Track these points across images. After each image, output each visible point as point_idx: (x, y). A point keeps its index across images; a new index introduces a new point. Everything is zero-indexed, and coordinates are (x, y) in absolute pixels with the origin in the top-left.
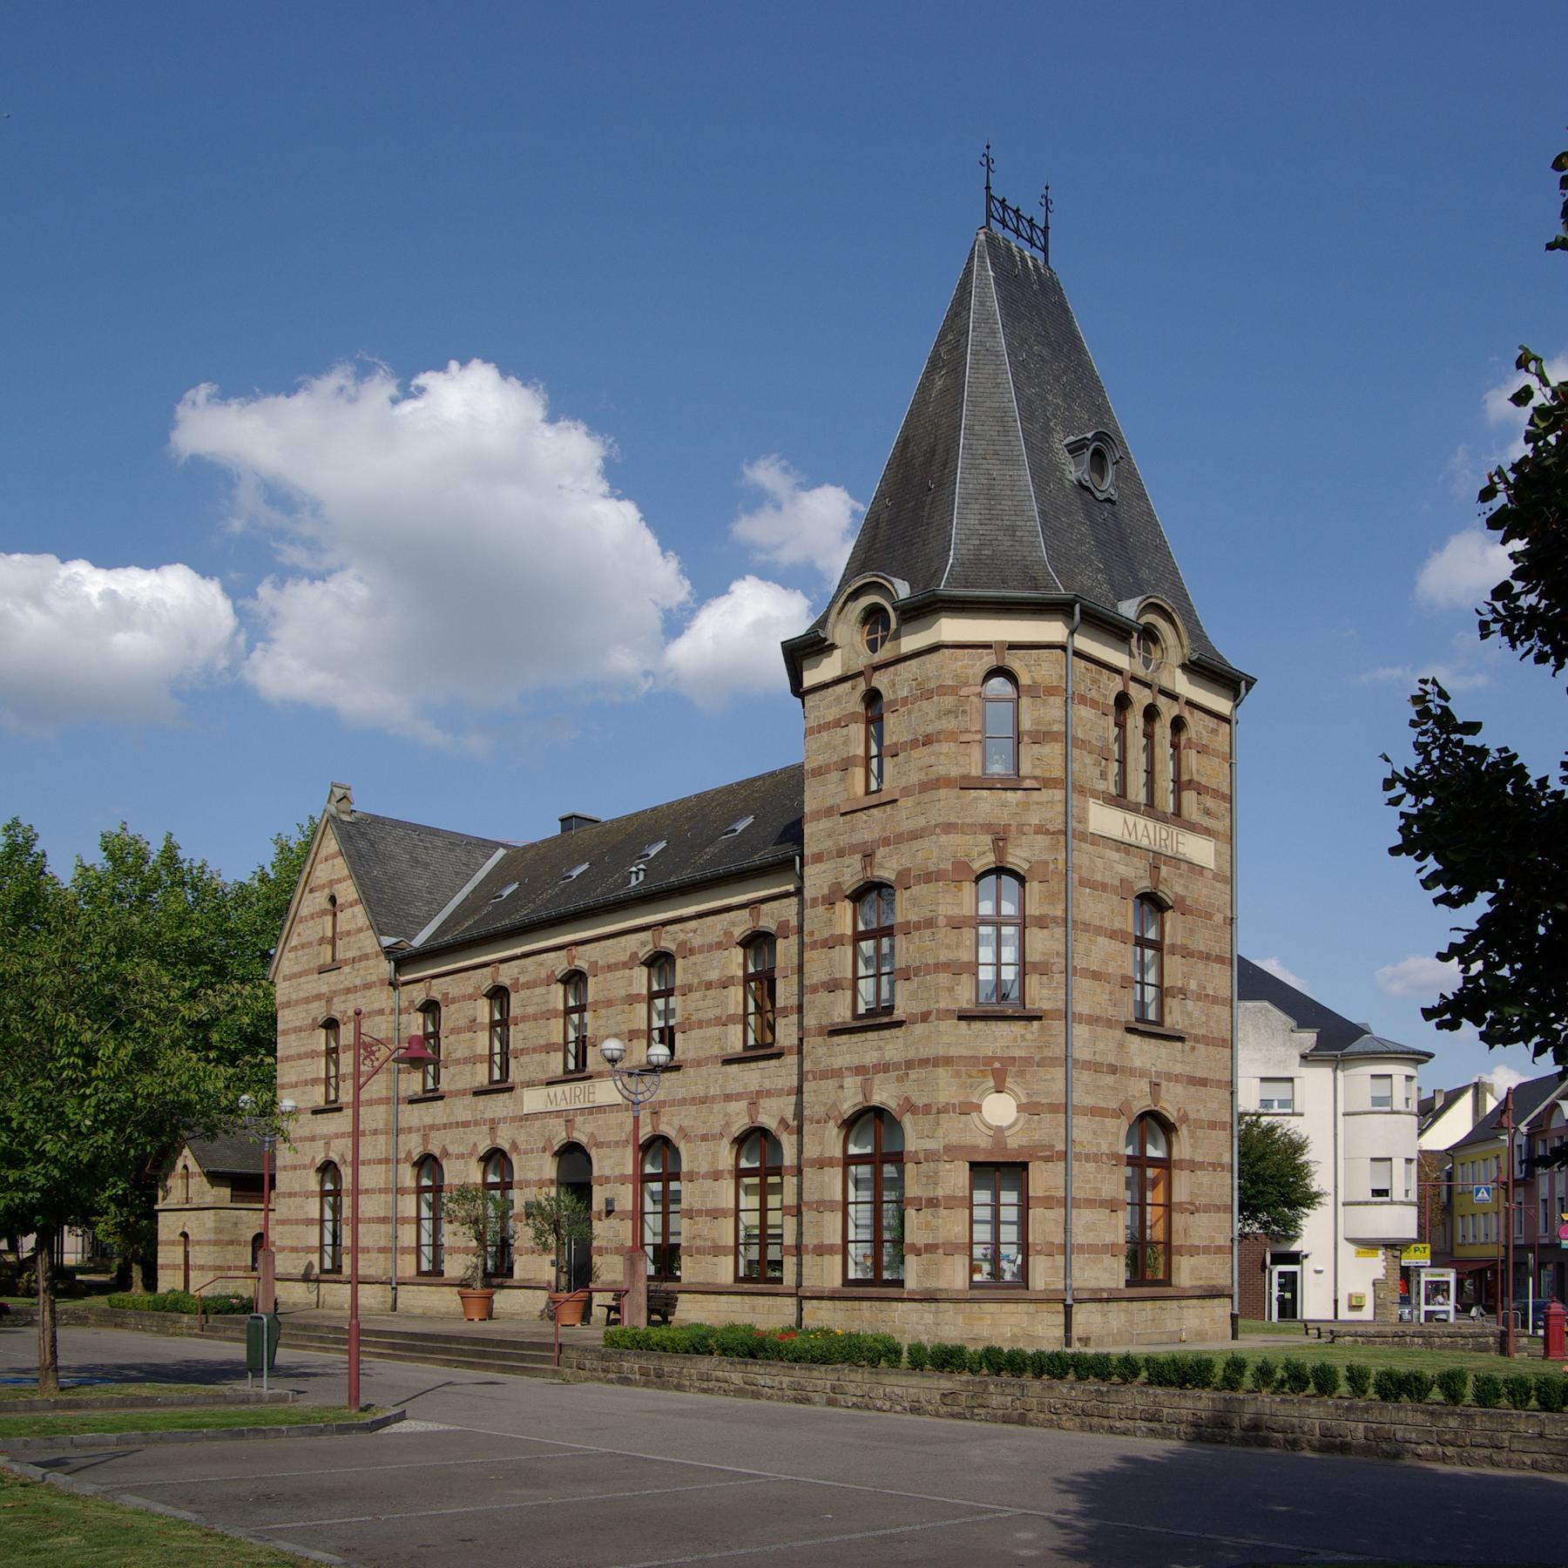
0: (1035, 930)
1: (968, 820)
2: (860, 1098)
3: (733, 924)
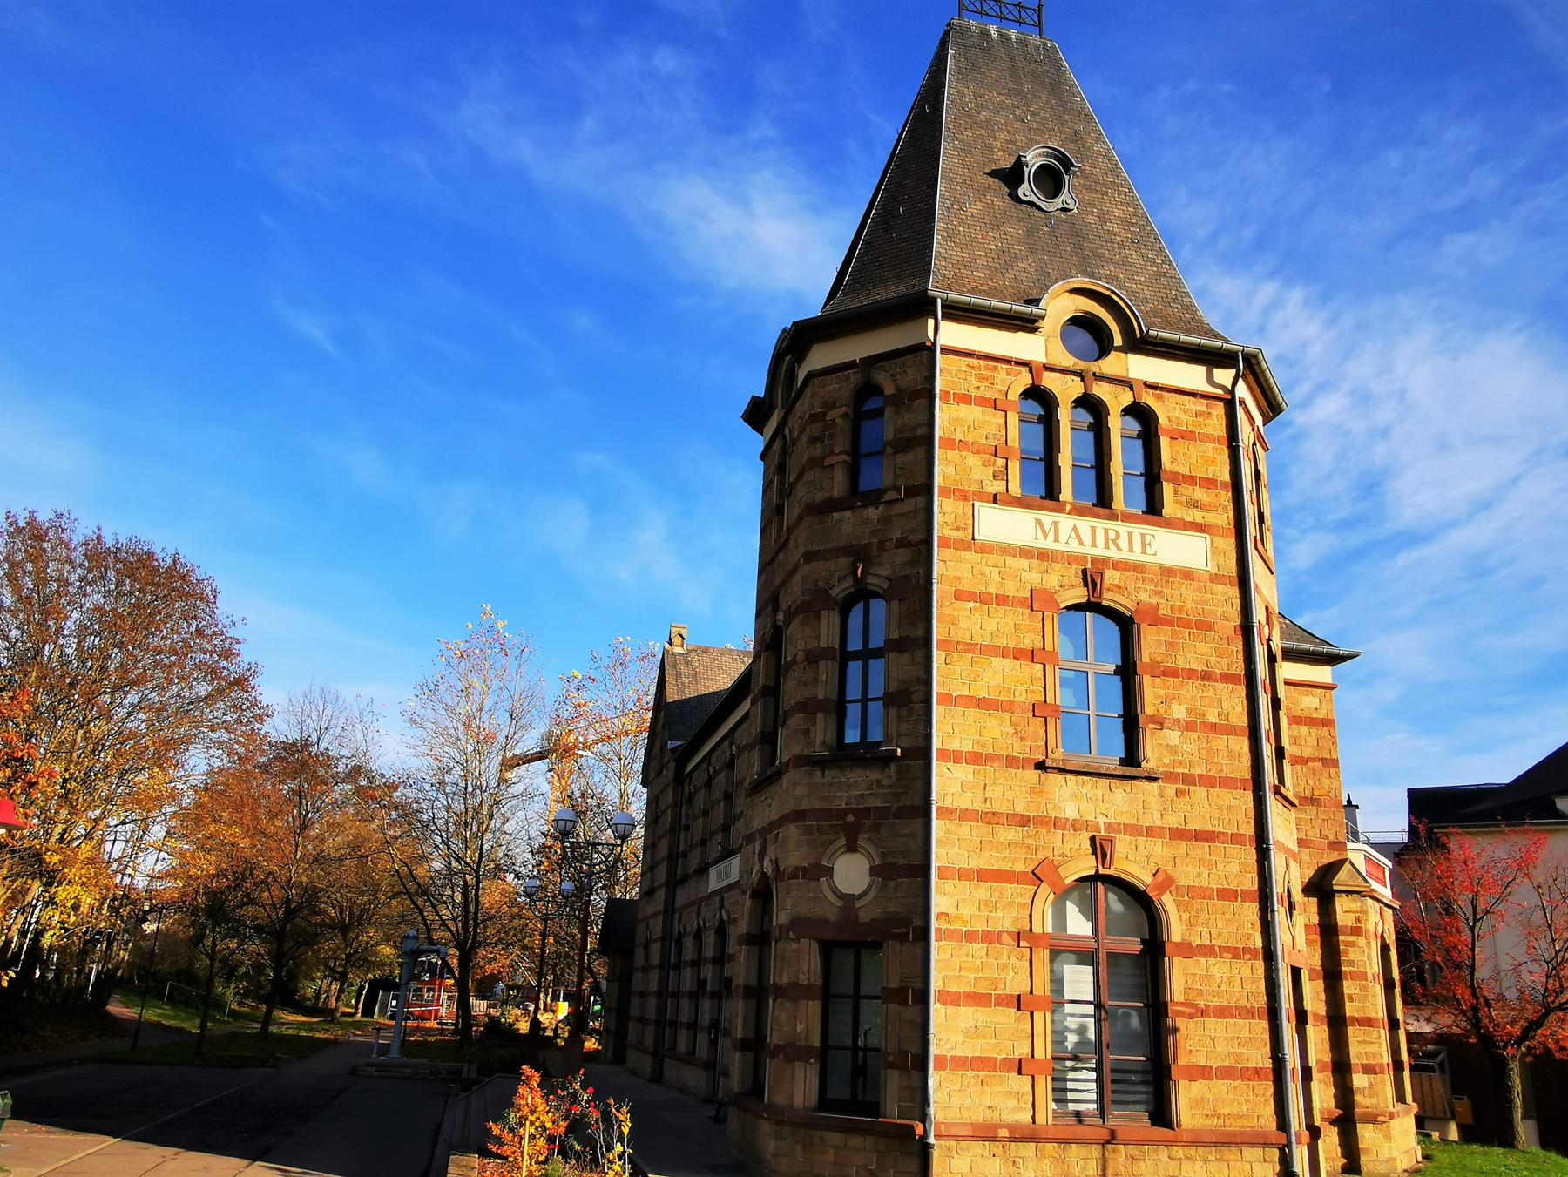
1: (829, 546)
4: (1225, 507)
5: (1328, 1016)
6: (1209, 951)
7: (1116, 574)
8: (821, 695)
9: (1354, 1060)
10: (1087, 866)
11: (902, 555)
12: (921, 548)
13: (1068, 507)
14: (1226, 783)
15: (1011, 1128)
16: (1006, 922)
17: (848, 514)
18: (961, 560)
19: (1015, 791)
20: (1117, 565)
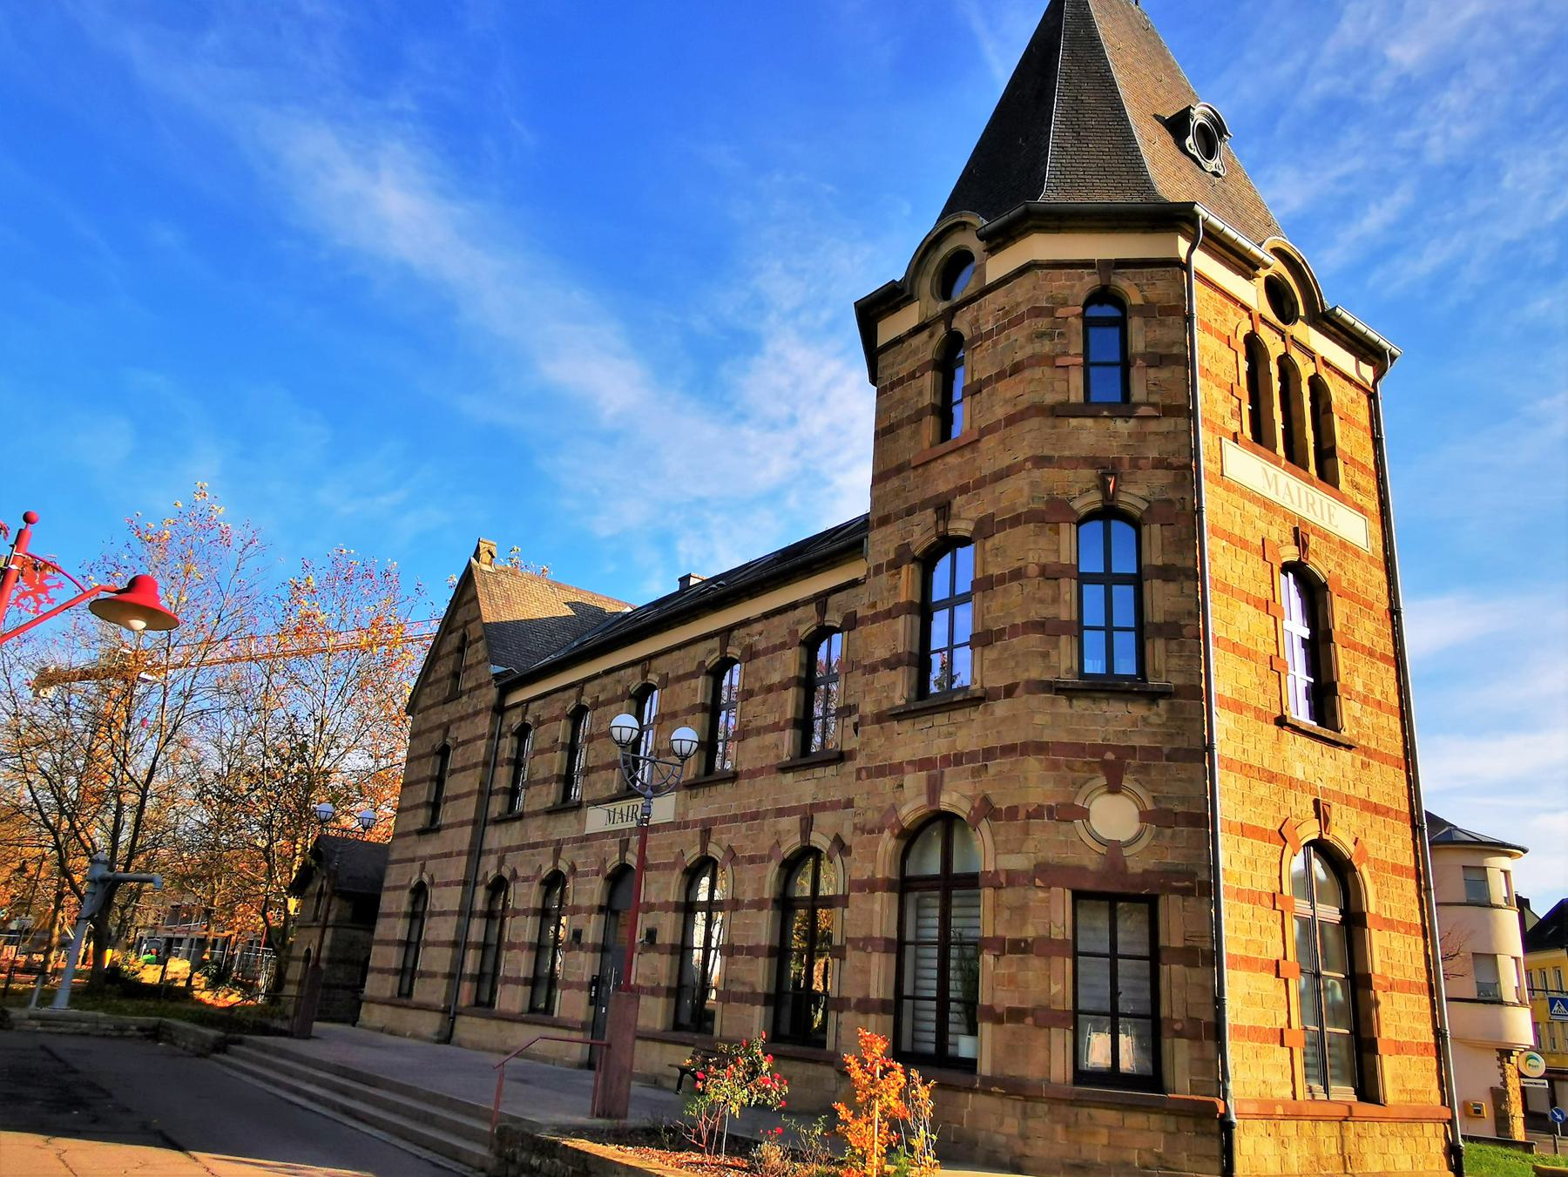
0: (1157, 583)
1: (1067, 453)
2: (923, 800)
3: (799, 622)
11: (1162, 478)
17: (1089, 422)
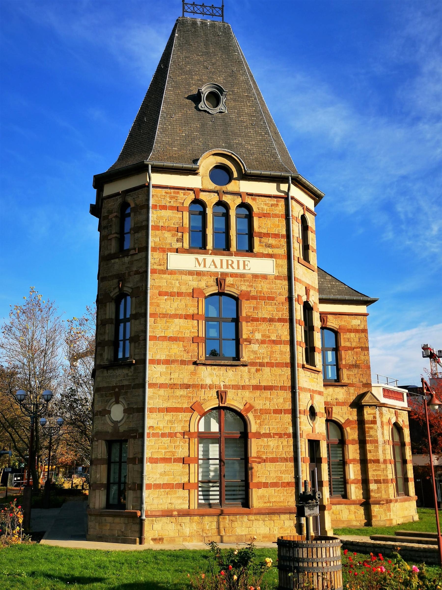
1: (110, 274)
4: (283, 246)
5: (360, 460)
6: (268, 435)
7: (231, 279)
8: (106, 339)
9: (371, 478)
10: (215, 403)
11: (137, 278)
12: (143, 275)
13: (210, 252)
14: (279, 365)
15: (179, 511)
16: (179, 428)
17: (117, 260)
18: (162, 278)
19: (183, 374)
20: (232, 275)
